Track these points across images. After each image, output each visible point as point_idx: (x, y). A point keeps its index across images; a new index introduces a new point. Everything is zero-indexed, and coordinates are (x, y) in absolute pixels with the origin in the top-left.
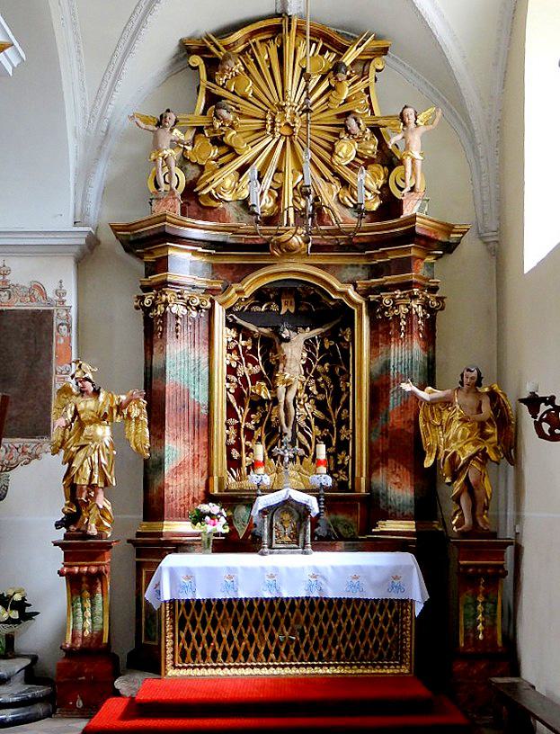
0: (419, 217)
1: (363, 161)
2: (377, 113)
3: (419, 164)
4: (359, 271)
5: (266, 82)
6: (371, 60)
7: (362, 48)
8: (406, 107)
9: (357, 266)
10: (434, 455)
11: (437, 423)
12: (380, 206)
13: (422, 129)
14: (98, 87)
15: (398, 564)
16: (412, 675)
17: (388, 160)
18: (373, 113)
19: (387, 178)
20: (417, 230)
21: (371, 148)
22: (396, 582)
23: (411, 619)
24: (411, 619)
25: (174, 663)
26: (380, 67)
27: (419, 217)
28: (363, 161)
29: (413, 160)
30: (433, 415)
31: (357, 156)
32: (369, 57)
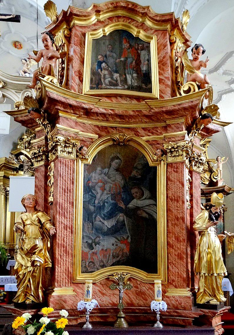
0: (227, 186)
1: (205, 171)
2: (208, 158)
3: (222, 172)
4: (119, 214)
5: (165, 278)
6: (206, 144)
7: (204, 141)
8: (218, 156)
9: (203, 199)
10: (231, 251)
11: (232, 242)
12: (209, 183)
13: (223, 163)
14: (37, 12)
15: (225, 281)
16: (229, 312)
17: (211, 171)
18: (207, 158)
19: (211, 175)
20: (225, 189)
21: (206, 167)
22: (225, 286)
23: (229, 297)
24: (229, 297)
25: (177, 156)
26: (208, 146)
27: (227, 186)
28: (205, 171)
29: (220, 170)
30: (230, 240)
31: (203, 170)
32: (205, 143)
